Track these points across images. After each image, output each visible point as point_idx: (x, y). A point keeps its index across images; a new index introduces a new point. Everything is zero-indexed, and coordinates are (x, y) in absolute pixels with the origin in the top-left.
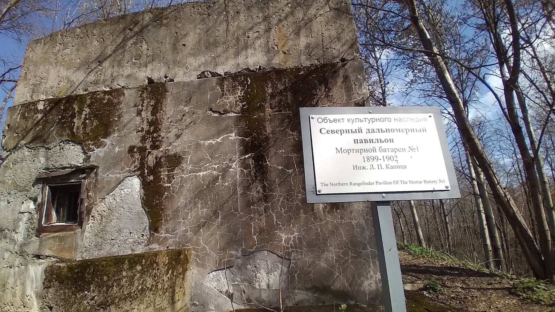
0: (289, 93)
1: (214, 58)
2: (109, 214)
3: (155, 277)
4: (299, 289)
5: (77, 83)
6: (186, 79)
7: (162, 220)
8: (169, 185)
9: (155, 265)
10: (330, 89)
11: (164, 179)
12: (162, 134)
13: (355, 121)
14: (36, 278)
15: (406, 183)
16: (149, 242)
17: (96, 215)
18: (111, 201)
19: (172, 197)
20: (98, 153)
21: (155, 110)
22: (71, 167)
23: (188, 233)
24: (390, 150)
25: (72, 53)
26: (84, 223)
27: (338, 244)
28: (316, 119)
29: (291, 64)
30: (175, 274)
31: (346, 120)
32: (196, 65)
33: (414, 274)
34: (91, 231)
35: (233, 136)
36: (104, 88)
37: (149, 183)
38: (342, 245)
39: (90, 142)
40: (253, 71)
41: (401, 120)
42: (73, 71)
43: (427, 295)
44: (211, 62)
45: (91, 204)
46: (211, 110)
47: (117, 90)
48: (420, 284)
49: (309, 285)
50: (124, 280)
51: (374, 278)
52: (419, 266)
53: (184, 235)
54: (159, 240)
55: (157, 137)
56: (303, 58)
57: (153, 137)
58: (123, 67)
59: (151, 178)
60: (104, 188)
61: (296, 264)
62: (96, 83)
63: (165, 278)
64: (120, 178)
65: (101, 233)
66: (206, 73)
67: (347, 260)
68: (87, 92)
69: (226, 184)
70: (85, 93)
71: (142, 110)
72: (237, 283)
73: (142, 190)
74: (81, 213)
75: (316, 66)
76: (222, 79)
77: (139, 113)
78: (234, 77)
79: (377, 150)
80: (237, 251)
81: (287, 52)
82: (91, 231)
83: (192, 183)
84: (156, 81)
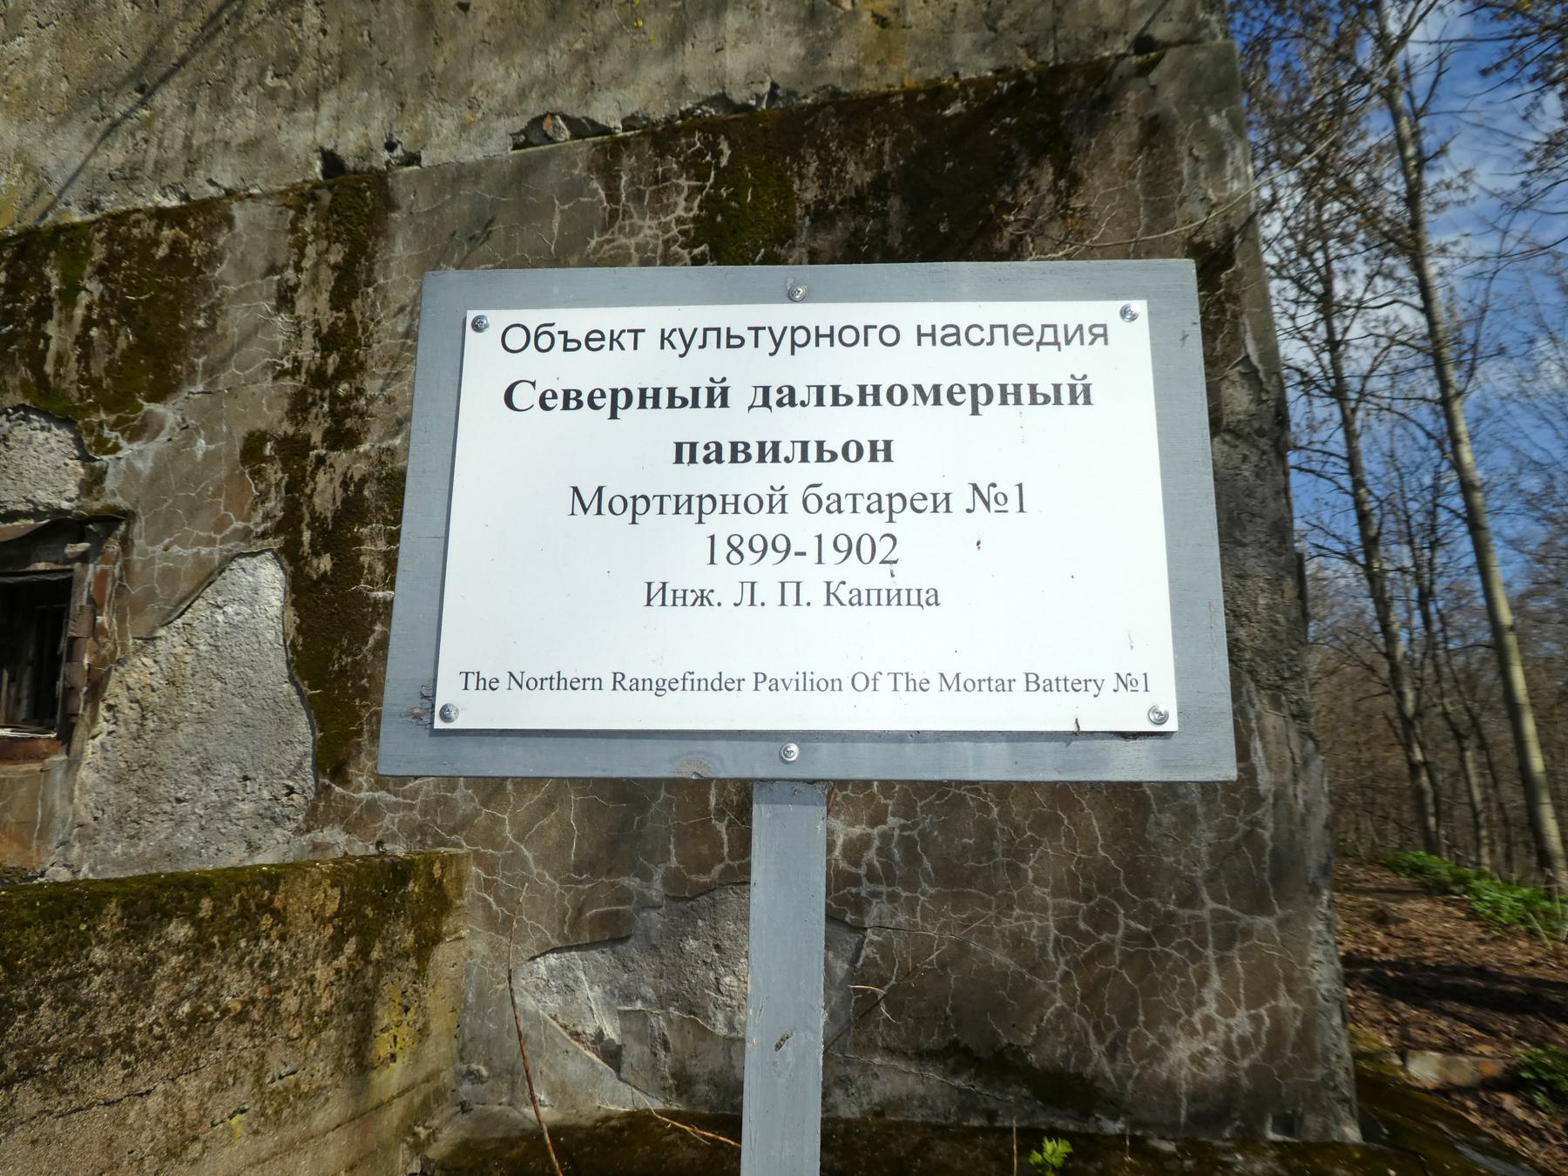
0: (895, 203)
1: (582, 57)
2: (169, 698)
3: (266, 965)
4: (890, 1051)
5: (60, 180)
6: (471, 153)
7: (359, 733)
9: (266, 921)
10: (1075, 181)
11: (372, 570)
12: (372, 386)
13: (698, 340)
15: (922, 686)
16: (314, 818)
17: (123, 703)
18: (179, 650)
20: (135, 457)
21: (348, 284)
22: (35, 514)
23: (457, 795)
24: (862, 504)
25: (37, 55)
26: (80, 732)
27: (1073, 877)
28: (493, 334)
29: (903, 72)
30: (375, 955)
31: (650, 340)
32: (509, 88)
33: (1468, 1010)
34: (101, 764)
36: (158, 198)
37: (317, 583)
38: (1087, 878)
39: (103, 416)
40: (745, 108)
41: (954, 336)
42: (42, 127)
43: (1520, 1114)
44: (569, 74)
45: (103, 661)
47: (207, 205)
48: (1486, 1059)
49: (934, 1041)
50: (97, 980)
51: (1221, 1029)
52: (1498, 977)
53: (442, 801)
54: (347, 812)
55: (349, 398)
56: (964, 40)
57: (335, 398)
58: (227, 109)
59: (325, 563)
60: (150, 596)
61: (884, 948)
62: (129, 176)
63: (322, 973)
64: (211, 561)
65: (137, 775)
66: (547, 125)
67: (1105, 950)
68: (98, 214)
70: (90, 217)
71: (294, 289)
72: (639, 1005)
73: (291, 612)
74: (71, 691)
75: (1020, 75)
76: (611, 151)
77: (285, 299)
78: (659, 137)
79: (794, 503)
80: (646, 876)
81: (892, 17)
82: (101, 764)
84: (350, 164)
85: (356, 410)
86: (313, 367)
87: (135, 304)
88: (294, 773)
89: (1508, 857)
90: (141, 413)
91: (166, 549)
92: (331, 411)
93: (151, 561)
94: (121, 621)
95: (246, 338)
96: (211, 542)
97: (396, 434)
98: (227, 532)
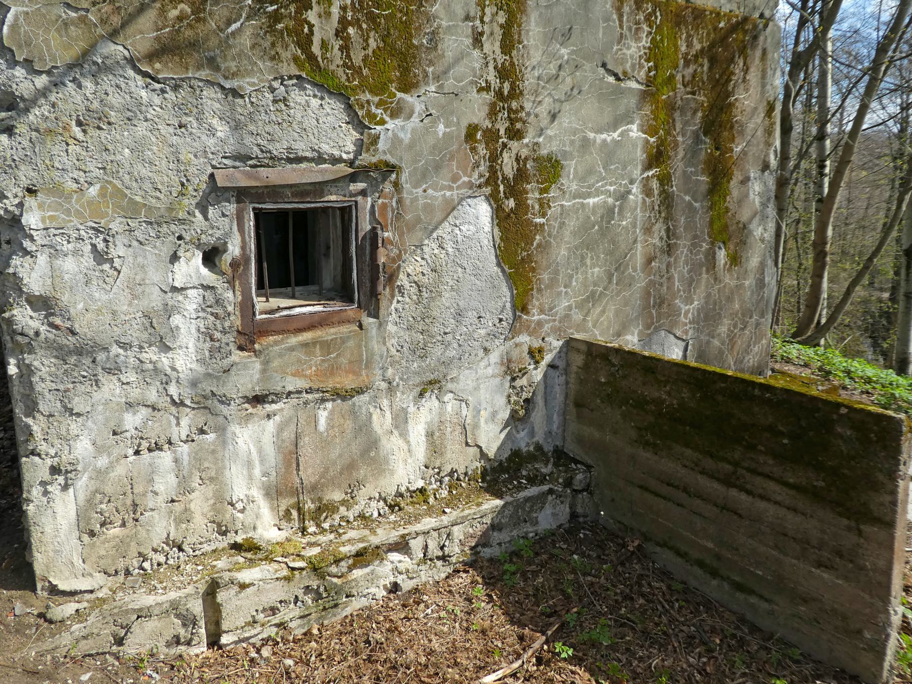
7: (532, 289)
8: (542, 220)
11: (533, 208)
12: (528, 106)
14: (260, 451)
17: (407, 285)
19: (548, 244)
23: (573, 312)
26: (383, 304)
35: (635, 131)
37: (509, 215)
46: (604, 65)
54: (529, 327)
57: (510, 110)
59: (511, 203)
64: (453, 200)
69: (624, 223)
73: (496, 230)
83: (578, 219)
85: (521, 119)
86: (497, 89)
87: (378, 16)
88: (502, 311)
89: (669, 249)
90: (396, 99)
91: (425, 191)
92: (509, 117)
93: (416, 199)
94: (401, 235)
95: (457, 61)
96: (450, 188)
97: (540, 135)
98: (460, 183)
